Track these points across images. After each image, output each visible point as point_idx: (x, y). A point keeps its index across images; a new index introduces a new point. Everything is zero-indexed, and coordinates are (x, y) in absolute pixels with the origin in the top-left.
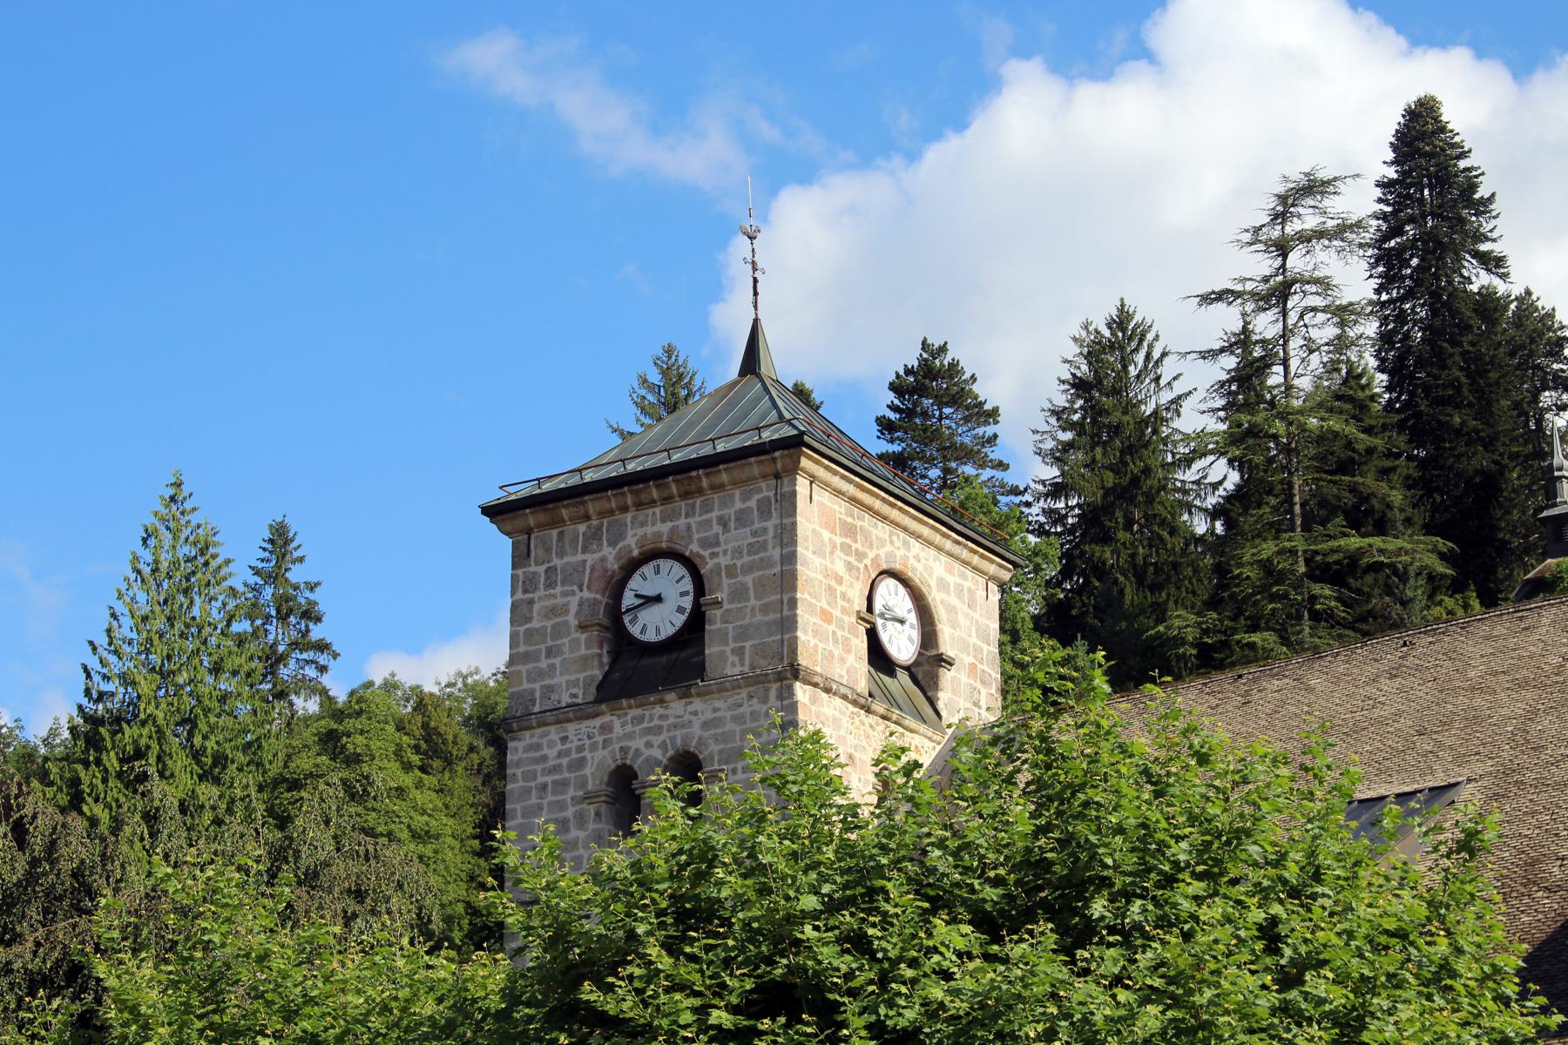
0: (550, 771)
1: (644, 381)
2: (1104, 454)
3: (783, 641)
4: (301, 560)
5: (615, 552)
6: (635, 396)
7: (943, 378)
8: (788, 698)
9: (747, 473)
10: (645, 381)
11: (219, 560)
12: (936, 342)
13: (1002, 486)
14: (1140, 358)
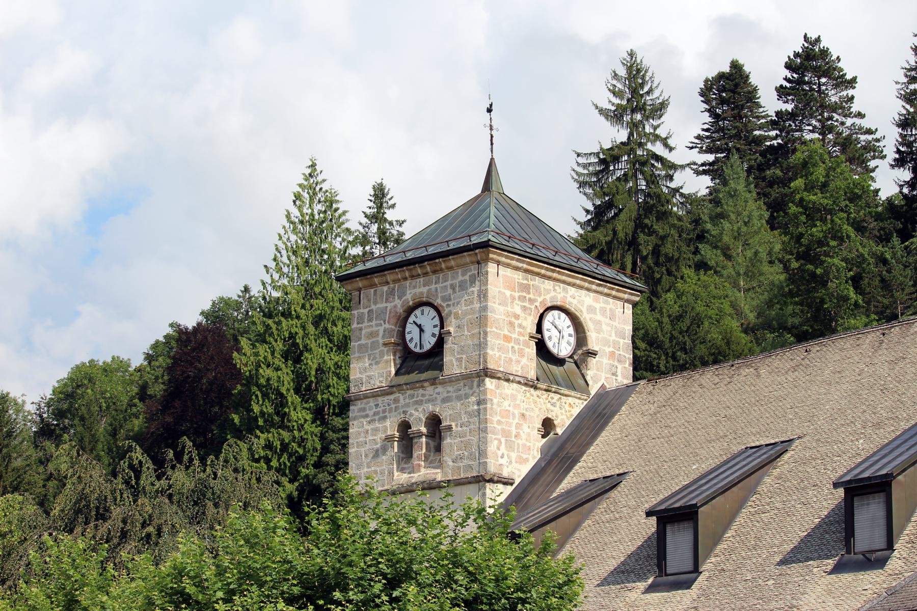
1: (615, 76)
4: (393, 206)
6: (609, 85)
10: (616, 75)
11: (340, 211)
12: (813, 36)
13: (860, 128)
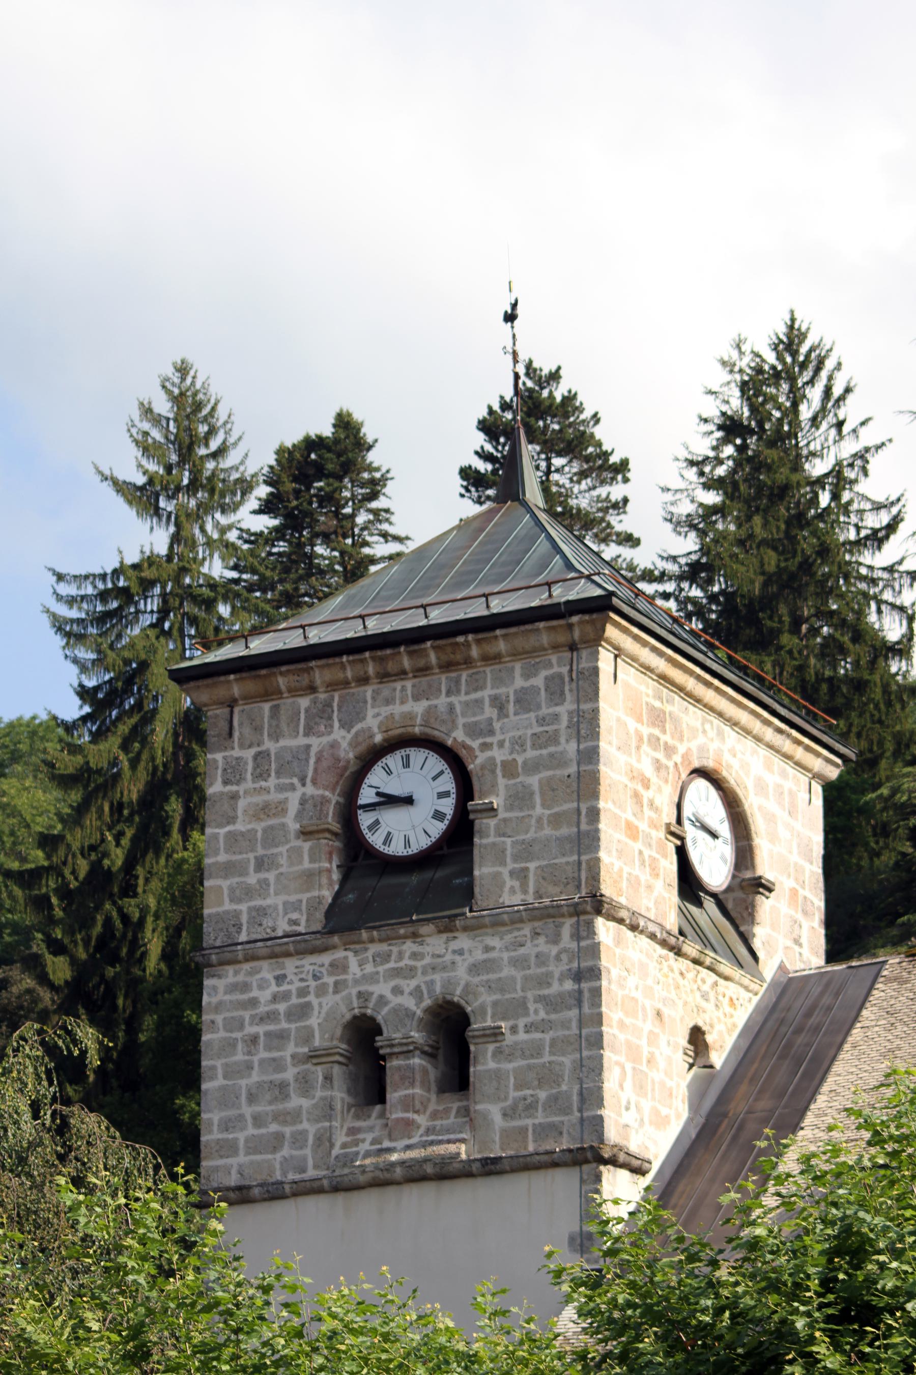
0: (262, 1019)
1: (147, 411)
2: (765, 525)
3: (579, 863)
5: (349, 736)
7: (554, 416)
8: (587, 937)
9: (532, 641)
12: (546, 367)
13: (631, 568)
14: (815, 394)
